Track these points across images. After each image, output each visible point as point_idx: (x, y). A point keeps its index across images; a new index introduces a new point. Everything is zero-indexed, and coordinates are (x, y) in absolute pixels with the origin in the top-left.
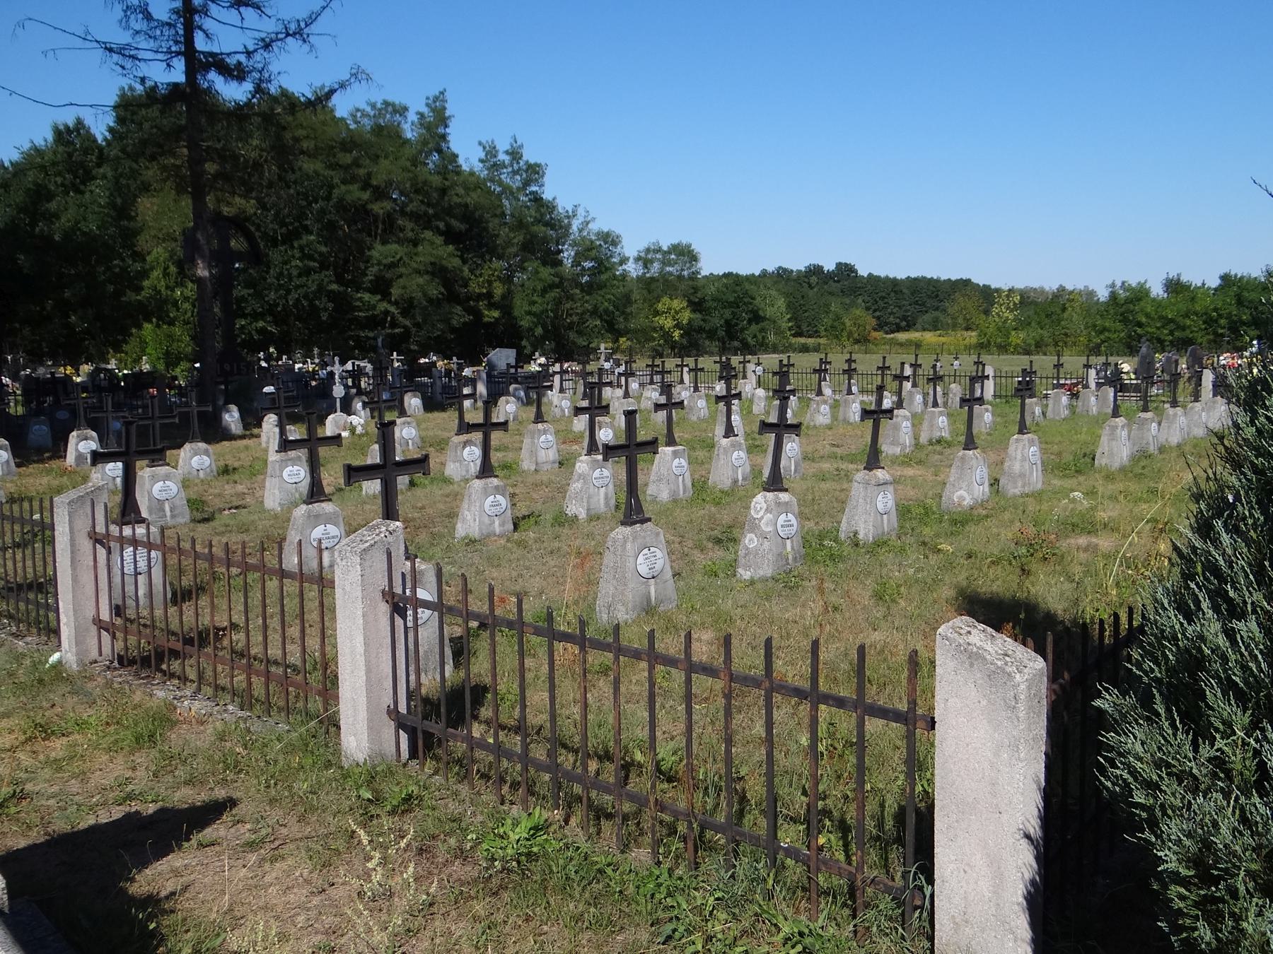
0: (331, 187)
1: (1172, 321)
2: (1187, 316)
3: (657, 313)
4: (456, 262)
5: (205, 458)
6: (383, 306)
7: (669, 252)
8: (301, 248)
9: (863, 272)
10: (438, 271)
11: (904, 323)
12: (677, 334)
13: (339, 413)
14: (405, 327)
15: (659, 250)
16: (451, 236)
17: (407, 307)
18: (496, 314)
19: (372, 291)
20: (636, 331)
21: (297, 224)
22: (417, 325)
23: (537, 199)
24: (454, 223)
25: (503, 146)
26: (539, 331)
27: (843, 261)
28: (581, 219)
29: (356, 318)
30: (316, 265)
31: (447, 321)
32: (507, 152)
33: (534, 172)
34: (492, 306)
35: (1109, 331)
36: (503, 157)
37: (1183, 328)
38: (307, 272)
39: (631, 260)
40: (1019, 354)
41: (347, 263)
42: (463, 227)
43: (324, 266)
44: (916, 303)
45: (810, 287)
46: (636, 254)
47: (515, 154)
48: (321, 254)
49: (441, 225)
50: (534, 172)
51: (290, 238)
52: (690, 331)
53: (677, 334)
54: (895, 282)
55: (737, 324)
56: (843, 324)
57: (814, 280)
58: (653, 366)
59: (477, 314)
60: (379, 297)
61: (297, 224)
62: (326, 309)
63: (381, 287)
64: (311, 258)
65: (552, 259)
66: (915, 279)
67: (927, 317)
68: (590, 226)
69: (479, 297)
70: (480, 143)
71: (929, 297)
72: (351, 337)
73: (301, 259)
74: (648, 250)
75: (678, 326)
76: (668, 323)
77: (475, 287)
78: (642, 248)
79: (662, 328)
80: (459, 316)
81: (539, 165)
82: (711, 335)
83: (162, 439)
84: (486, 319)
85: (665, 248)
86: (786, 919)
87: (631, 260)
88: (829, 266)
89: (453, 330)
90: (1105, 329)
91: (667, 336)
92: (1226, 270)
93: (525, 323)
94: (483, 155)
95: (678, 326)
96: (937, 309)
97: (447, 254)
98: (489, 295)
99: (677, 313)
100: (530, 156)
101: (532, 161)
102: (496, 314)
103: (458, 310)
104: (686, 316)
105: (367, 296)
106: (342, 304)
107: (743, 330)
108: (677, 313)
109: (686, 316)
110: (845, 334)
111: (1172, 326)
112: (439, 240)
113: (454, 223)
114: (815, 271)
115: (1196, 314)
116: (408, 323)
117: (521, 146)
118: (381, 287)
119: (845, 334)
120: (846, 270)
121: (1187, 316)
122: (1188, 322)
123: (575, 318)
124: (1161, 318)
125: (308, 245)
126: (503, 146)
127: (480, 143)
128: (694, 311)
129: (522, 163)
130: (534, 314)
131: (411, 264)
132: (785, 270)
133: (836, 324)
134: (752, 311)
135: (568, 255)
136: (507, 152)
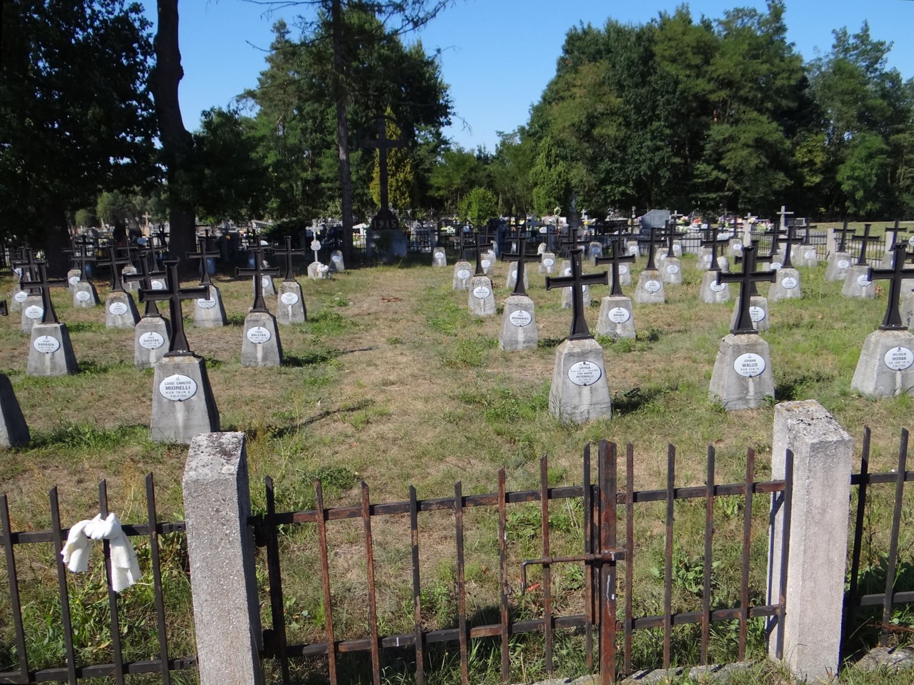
0: (677, 83)
5: (86, 293)
10: (760, 144)
13: (316, 262)
16: (778, 115)
17: (739, 175)
25: (663, 12)
26: (860, 194)
29: (695, 185)
33: (877, 51)
34: (814, 172)
41: (692, 144)
42: (793, 105)
49: (769, 105)
50: (877, 51)
51: (644, 124)
59: (800, 179)
63: (716, 160)
69: (804, 164)
72: (693, 199)
73: (652, 140)
77: (800, 156)
80: (781, 180)
83: (49, 276)
94: (834, 42)
97: (772, 130)
98: (811, 163)
100: (874, 37)
102: (817, 179)
103: (781, 175)
113: (784, 103)
118: (716, 160)
126: (854, 29)
127: (834, 31)
130: (857, 179)
131: (739, 137)
136: (856, 37)
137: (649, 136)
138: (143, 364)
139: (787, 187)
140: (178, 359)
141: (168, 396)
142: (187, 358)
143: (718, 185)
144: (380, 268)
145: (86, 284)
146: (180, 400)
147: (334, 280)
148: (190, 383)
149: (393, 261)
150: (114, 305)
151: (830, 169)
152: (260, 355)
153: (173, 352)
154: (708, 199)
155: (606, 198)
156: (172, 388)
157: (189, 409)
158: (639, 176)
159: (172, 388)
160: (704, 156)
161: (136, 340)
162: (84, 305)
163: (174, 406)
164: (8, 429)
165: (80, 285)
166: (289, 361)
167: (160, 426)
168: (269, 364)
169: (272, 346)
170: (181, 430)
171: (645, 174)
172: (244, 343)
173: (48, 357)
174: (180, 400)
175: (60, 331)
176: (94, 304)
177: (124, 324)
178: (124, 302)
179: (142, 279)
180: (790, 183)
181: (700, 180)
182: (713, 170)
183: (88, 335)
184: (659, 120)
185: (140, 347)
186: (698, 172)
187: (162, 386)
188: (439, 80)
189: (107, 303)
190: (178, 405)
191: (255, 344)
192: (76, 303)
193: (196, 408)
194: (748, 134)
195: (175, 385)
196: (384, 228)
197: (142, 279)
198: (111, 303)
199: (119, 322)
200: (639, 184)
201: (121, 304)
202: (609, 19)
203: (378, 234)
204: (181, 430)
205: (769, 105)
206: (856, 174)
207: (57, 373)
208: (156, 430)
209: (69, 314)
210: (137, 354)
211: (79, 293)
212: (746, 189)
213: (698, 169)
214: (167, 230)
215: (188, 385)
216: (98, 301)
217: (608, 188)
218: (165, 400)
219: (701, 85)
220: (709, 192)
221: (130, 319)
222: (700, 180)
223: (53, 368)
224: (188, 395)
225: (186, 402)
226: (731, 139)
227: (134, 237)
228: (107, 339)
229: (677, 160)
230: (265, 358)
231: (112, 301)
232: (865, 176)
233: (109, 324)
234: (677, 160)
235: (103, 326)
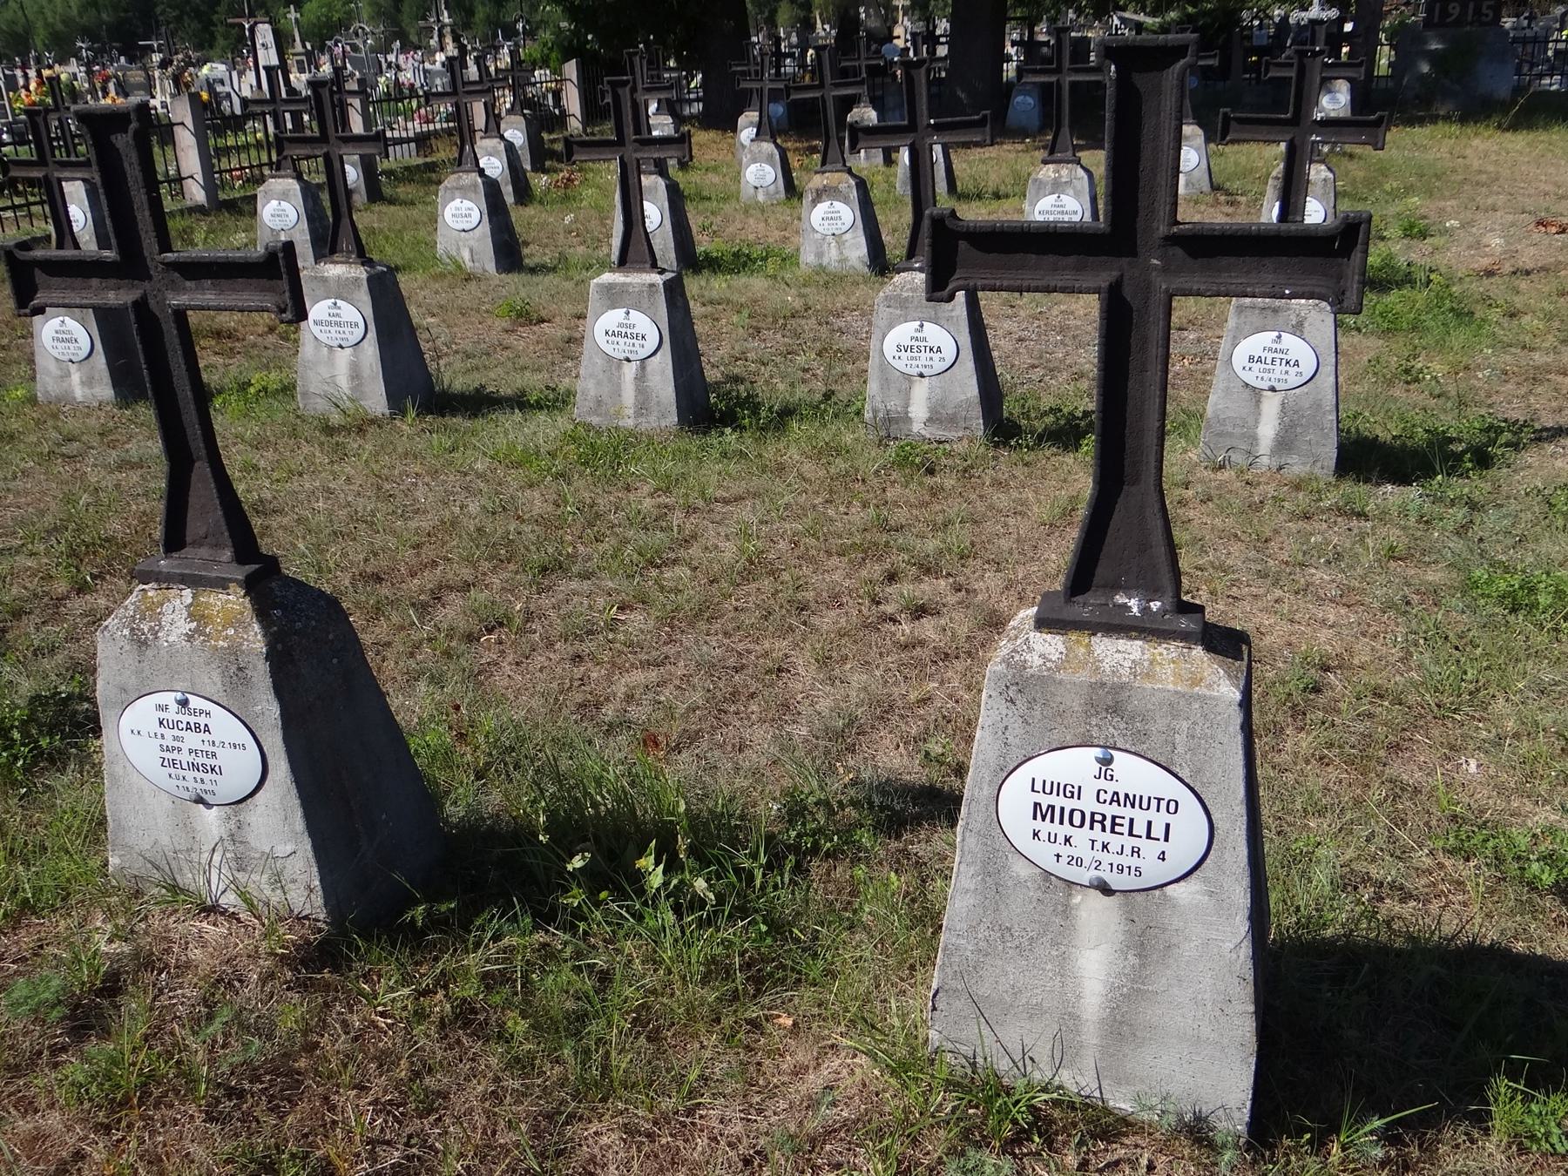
5: (768, 168)
138: (889, 420)
140: (1117, 655)
141: (1043, 854)
142: (1168, 652)
144: (1441, 129)
145: (768, 147)
146: (1105, 889)
147: (1351, 156)
148: (1173, 806)
149: (1476, 110)
150: (822, 208)
152: (1267, 430)
153: (1084, 608)
156: (1066, 817)
157: (1146, 939)
159: (1066, 817)
161: (874, 343)
162: (761, 198)
163: (1066, 911)
164: (316, 848)
165: (755, 147)
166: (1362, 458)
167: (983, 990)
168: (1297, 467)
169: (1317, 405)
170: (1091, 1036)
172: (1219, 380)
173: (630, 371)
174: (1105, 889)
175: (661, 299)
176: (782, 195)
177: (843, 260)
178: (846, 201)
179: (119, 296)
183: (756, 284)
185: (885, 366)
187: (1016, 799)
189: (807, 199)
190: (1092, 908)
191: (1256, 393)
192: (746, 192)
193: (1189, 949)
195: (1088, 804)
196: (1459, 22)
197: (119, 296)
198: (815, 202)
199: (831, 256)
201: (838, 205)
203: (1442, 39)
204: (1091, 1036)
207: (650, 423)
208: (961, 1004)
209: (727, 220)
210: (873, 387)
211: (753, 168)
214: (943, 26)
215: (1160, 820)
216: (792, 190)
218: (1021, 870)
221: (857, 250)
223: (642, 408)
224: (1154, 872)
225: (1141, 903)
227: (874, 47)
228: (798, 304)
230: (1284, 443)
231: (819, 196)
233: (808, 257)
235: (790, 260)
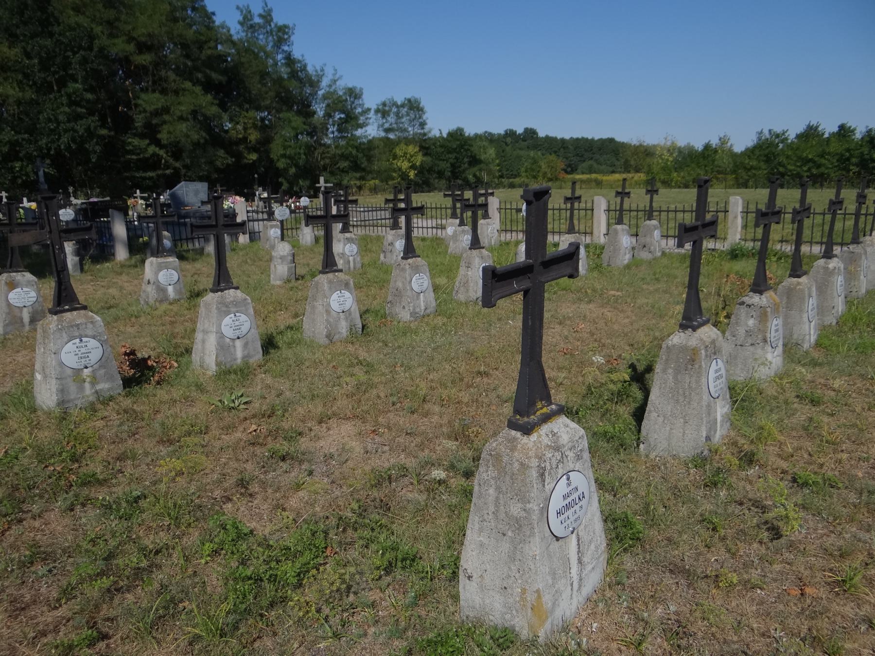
1: (811, 160)
2: (822, 156)
3: (395, 157)
4: (214, 109)
6: (152, 149)
7: (403, 106)
8: (69, 96)
9: (542, 134)
11: (569, 169)
12: (412, 174)
14: (175, 169)
15: (395, 104)
16: (208, 86)
18: (254, 157)
19: (142, 136)
20: (379, 172)
21: (62, 73)
22: (186, 167)
23: (290, 60)
24: (214, 75)
25: (257, 10)
27: (529, 127)
28: (330, 77)
30: (84, 110)
31: (211, 163)
32: (260, 16)
35: (755, 169)
36: (257, 20)
37: (819, 166)
38: (78, 117)
39: (372, 112)
40: (679, 187)
42: (223, 79)
43: (91, 113)
44: (577, 155)
45: (506, 144)
46: (375, 107)
47: (267, 17)
48: (88, 101)
50: (282, 35)
52: (421, 170)
53: (412, 174)
54: (563, 140)
55: (460, 167)
56: (540, 167)
57: (509, 140)
58: (395, 201)
59: (239, 156)
60: (147, 141)
61: (62, 73)
62: (95, 152)
63: (151, 132)
64: (77, 104)
65: (306, 112)
66: (577, 139)
67: (585, 165)
68: (338, 83)
70: (238, 8)
71: (586, 150)
74: (384, 104)
75: (413, 167)
76: (405, 165)
78: (379, 102)
79: (400, 169)
81: (286, 26)
82: (440, 174)
84: (246, 161)
85: (399, 103)
86: (487, 374)
87: (372, 112)
88: (520, 130)
89: (218, 170)
90: (752, 168)
91: (404, 176)
92: (814, 123)
93: (281, 164)
94: (241, 18)
95: (413, 167)
96: (592, 159)
97: (206, 102)
99: (412, 156)
100: (279, 19)
101: (280, 23)
102: (254, 157)
103: (221, 153)
104: (419, 159)
105: (136, 141)
106: (112, 149)
107: (464, 171)
108: (412, 156)
109: (419, 159)
110: (541, 174)
111: (811, 164)
112: (198, 89)
113: (214, 75)
114: (511, 134)
115: (829, 154)
116: (177, 165)
117: (270, 10)
119: (541, 174)
120: (530, 133)
121: (822, 156)
122: (823, 161)
123: (327, 161)
124: (800, 158)
125: (74, 93)
126: (257, 10)
127: (238, 8)
128: (425, 155)
129: (273, 25)
130: (290, 157)
132: (490, 134)
133: (534, 167)
134: (471, 156)
135: (320, 109)
136: (260, 16)
137: (64, 100)
139: (228, 165)
143: (153, 163)
151: (265, 143)
154: (144, 178)
155: (15, 178)
158: (58, 152)
160: (136, 128)
171: (68, 148)
180: (230, 160)
181: (134, 157)
182: (149, 145)
184: (76, 81)
186: (131, 147)
188: (44, 407)
194: (184, 107)
200: (58, 160)
202: (224, 22)
205: (200, 75)
206: (288, 153)
212: (186, 167)
213: (130, 143)
217: (18, 165)
219: (119, 47)
220: (145, 171)
222: (134, 157)
226: (166, 110)
229: (104, 132)
232: (295, 154)
234: (104, 132)
